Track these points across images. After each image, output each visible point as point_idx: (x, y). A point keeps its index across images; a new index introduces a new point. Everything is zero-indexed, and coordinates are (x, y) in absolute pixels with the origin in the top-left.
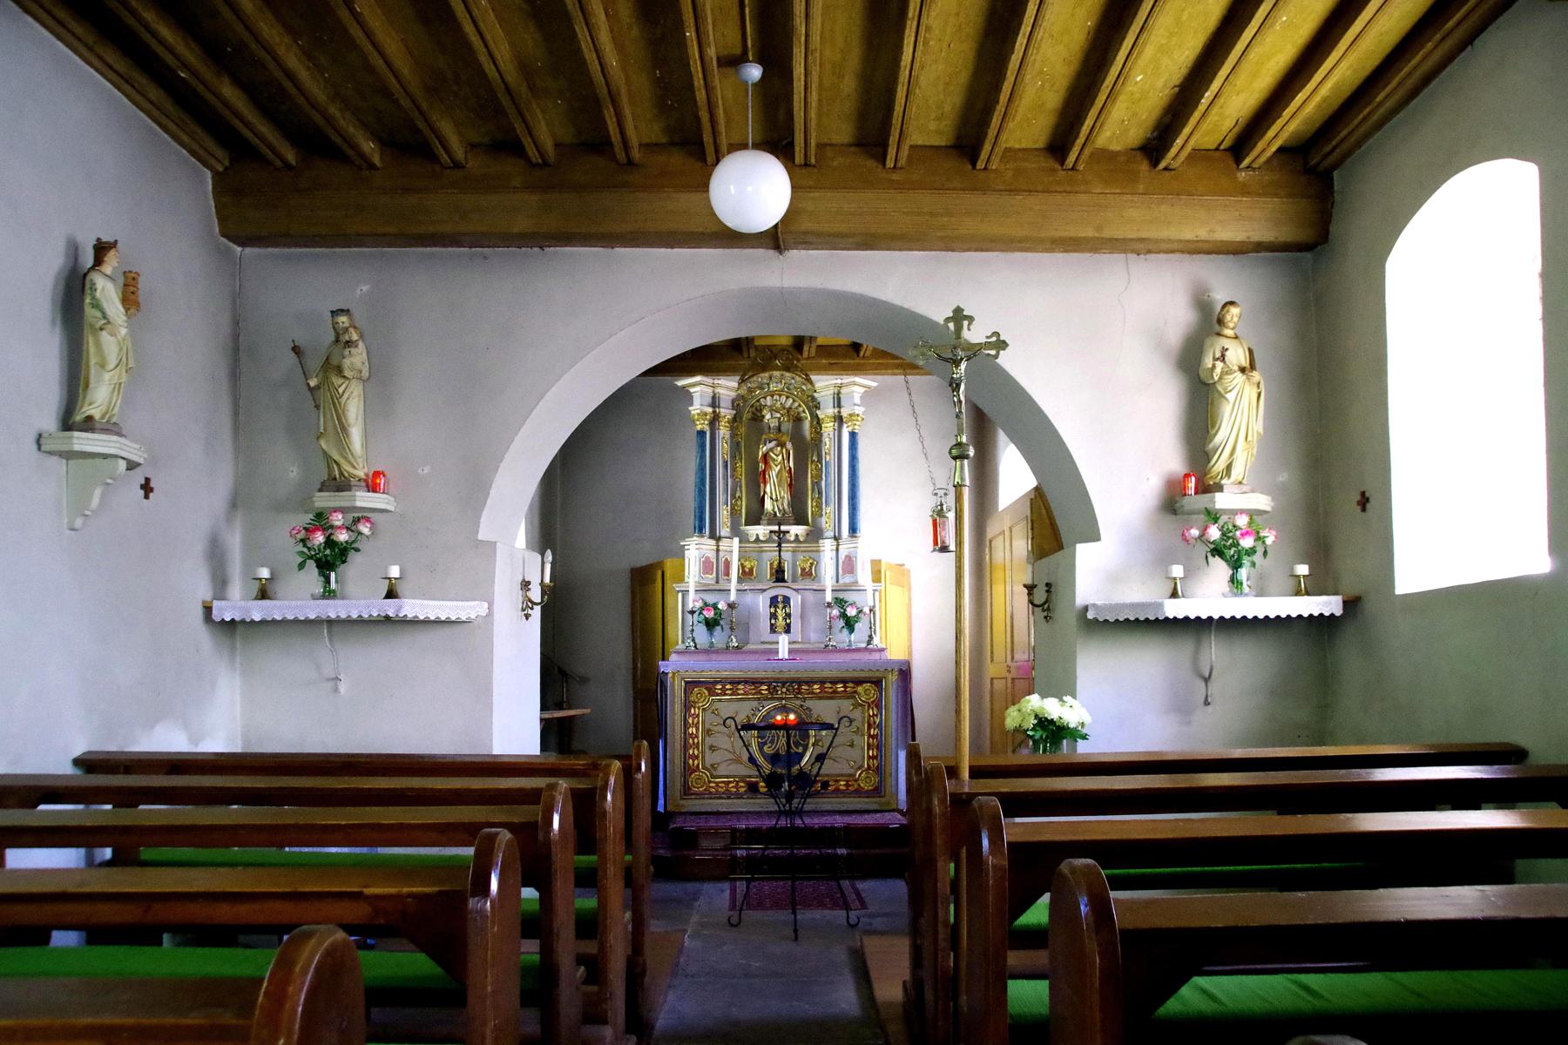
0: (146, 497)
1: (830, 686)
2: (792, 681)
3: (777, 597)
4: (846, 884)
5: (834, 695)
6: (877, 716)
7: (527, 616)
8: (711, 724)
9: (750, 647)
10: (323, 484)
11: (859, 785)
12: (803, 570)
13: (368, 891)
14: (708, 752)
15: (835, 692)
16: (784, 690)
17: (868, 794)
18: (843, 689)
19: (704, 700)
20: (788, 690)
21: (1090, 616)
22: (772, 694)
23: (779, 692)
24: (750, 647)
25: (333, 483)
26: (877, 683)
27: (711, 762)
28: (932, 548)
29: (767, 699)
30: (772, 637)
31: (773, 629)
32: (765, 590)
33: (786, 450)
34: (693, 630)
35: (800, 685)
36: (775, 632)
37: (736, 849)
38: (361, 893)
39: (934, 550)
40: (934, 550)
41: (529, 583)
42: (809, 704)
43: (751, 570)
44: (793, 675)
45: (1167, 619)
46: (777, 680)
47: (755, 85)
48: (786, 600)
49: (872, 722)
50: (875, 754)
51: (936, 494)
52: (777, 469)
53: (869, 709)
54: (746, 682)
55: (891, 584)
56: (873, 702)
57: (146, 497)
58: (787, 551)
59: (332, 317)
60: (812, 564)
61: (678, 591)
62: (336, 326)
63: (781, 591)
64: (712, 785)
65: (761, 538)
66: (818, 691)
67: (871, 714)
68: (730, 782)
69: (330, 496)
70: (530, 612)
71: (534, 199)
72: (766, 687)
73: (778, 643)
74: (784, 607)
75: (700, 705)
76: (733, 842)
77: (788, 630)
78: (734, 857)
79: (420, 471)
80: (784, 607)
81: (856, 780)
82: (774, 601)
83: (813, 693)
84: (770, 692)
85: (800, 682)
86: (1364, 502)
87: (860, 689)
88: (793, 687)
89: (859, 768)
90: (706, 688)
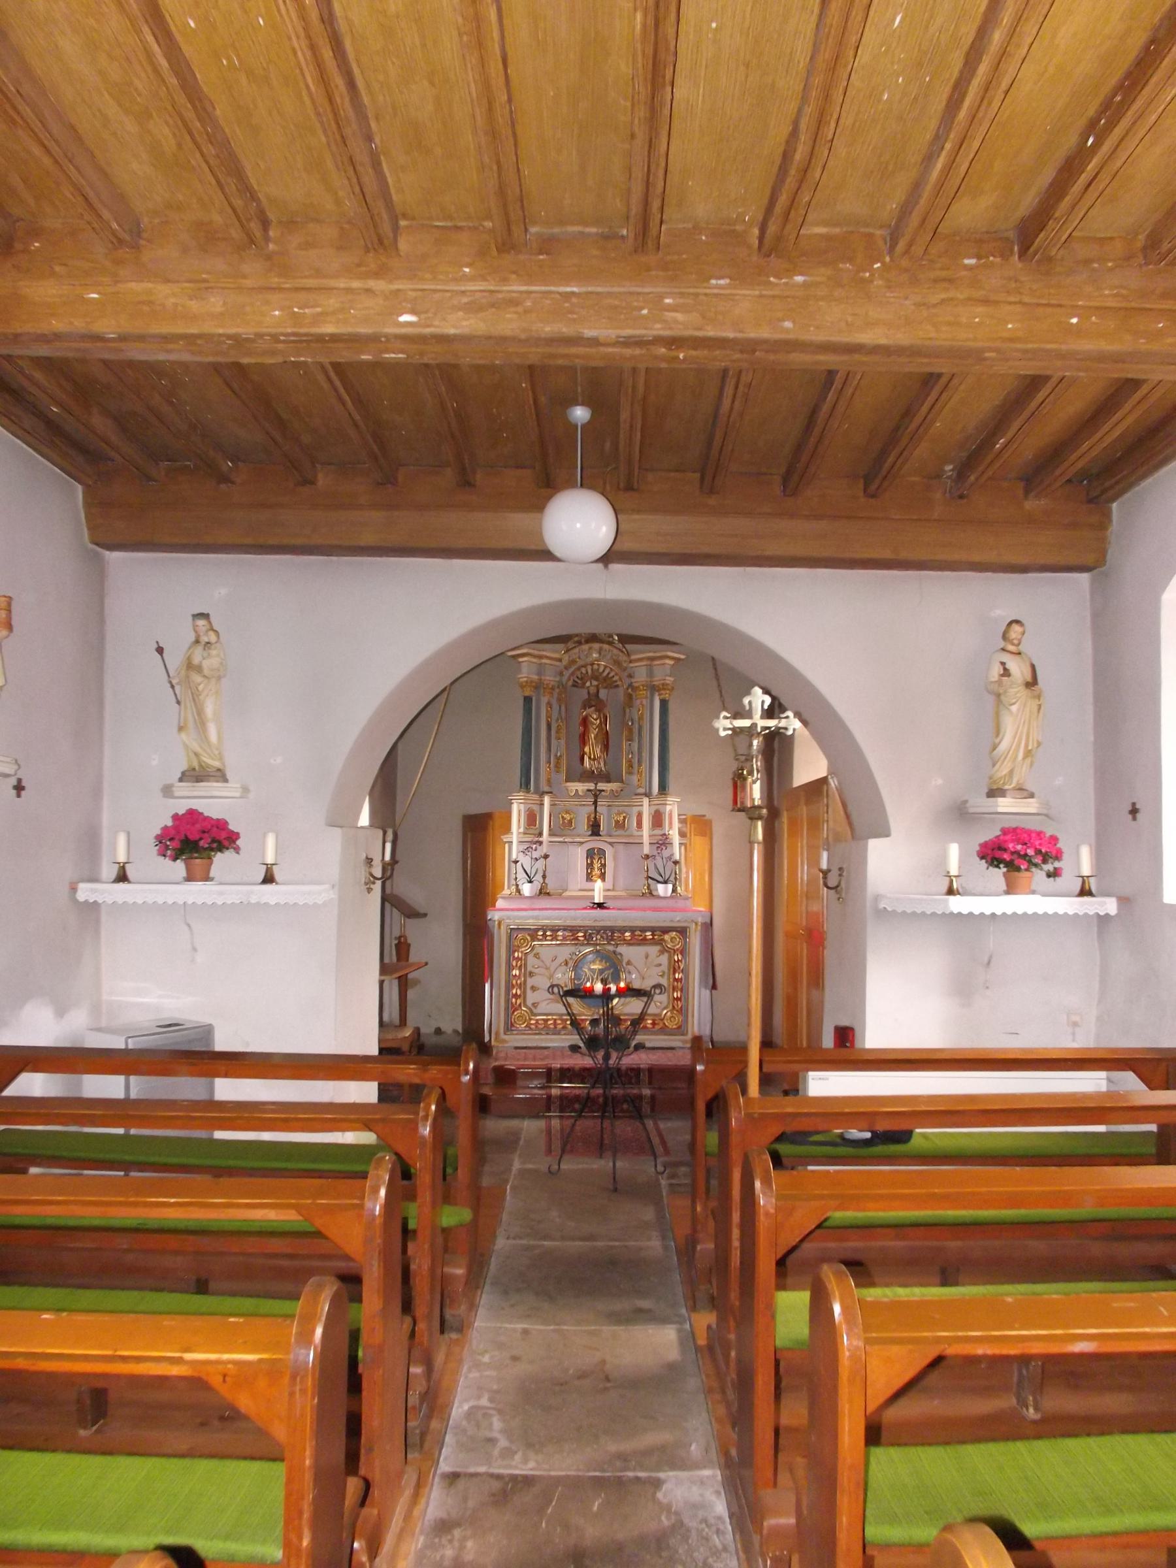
0: (19, 796)
1: (640, 933)
2: (605, 928)
3: (594, 849)
4: (650, 1123)
5: (644, 942)
6: (681, 961)
7: (369, 890)
8: (533, 967)
9: (567, 894)
10: (183, 773)
11: (664, 1024)
12: (617, 822)
13: (188, 1356)
14: (529, 991)
15: (645, 939)
16: (599, 937)
17: (672, 1033)
18: (651, 937)
19: (527, 946)
20: (601, 937)
21: (882, 906)
22: (588, 941)
23: (594, 939)
24: (567, 894)
25: (192, 773)
26: (683, 931)
27: (532, 1002)
28: (731, 807)
29: (583, 945)
30: (588, 885)
31: (589, 878)
32: (583, 843)
33: (604, 714)
34: (516, 878)
35: (613, 933)
36: (591, 880)
37: (550, 1087)
38: (181, 1358)
39: (733, 810)
40: (733, 810)
41: (372, 860)
42: (622, 949)
43: (570, 822)
44: (609, 924)
45: (952, 914)
46: (592, 928)
47: (583, 426)
48: (602, 853)
49: (677, 968)
50: (679, 996)
51: (737, 760)
52: (595, 732)
53: (674, 955)
54: (565, 929)
55: (695, 835)
56: (678, 949)
57: (19, 796)
58: (602, 805)
59: (193, 620)
60: (625, 817)
61: (506, 842)
62: (197, 628)
63: (596, 843)
64: (533, 1022)
65: (580, 793)
66: (629, 938)
67: (676, 959)
68: (549, 1020)
69: (188, 787)
70: (372, 886)
71: (378, 516)
72: (582, 934)
73: (594, 890)
74: (600, 858)
75: (523, 949)
76: (549, 1080)
77: (603, 876)
78: (549, 1097)
79: (272, 761)
80: (600, 858)
81: (662, 1020)
82: (590, 854)
83: (625, 940)
84: (585, 939)
85: (613, 930)
86: (1134, 811)
87: (667, 937)
88: (607, 934)
89: (665, 1008)
90: (529, 935)
